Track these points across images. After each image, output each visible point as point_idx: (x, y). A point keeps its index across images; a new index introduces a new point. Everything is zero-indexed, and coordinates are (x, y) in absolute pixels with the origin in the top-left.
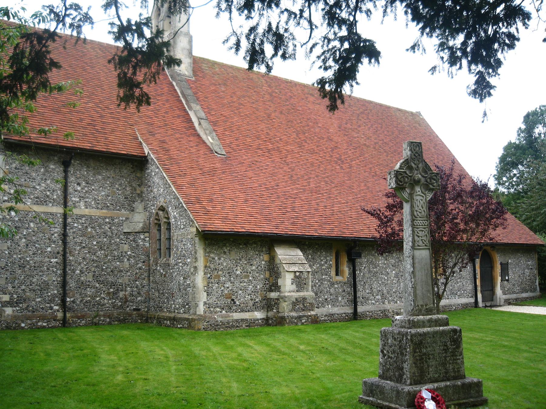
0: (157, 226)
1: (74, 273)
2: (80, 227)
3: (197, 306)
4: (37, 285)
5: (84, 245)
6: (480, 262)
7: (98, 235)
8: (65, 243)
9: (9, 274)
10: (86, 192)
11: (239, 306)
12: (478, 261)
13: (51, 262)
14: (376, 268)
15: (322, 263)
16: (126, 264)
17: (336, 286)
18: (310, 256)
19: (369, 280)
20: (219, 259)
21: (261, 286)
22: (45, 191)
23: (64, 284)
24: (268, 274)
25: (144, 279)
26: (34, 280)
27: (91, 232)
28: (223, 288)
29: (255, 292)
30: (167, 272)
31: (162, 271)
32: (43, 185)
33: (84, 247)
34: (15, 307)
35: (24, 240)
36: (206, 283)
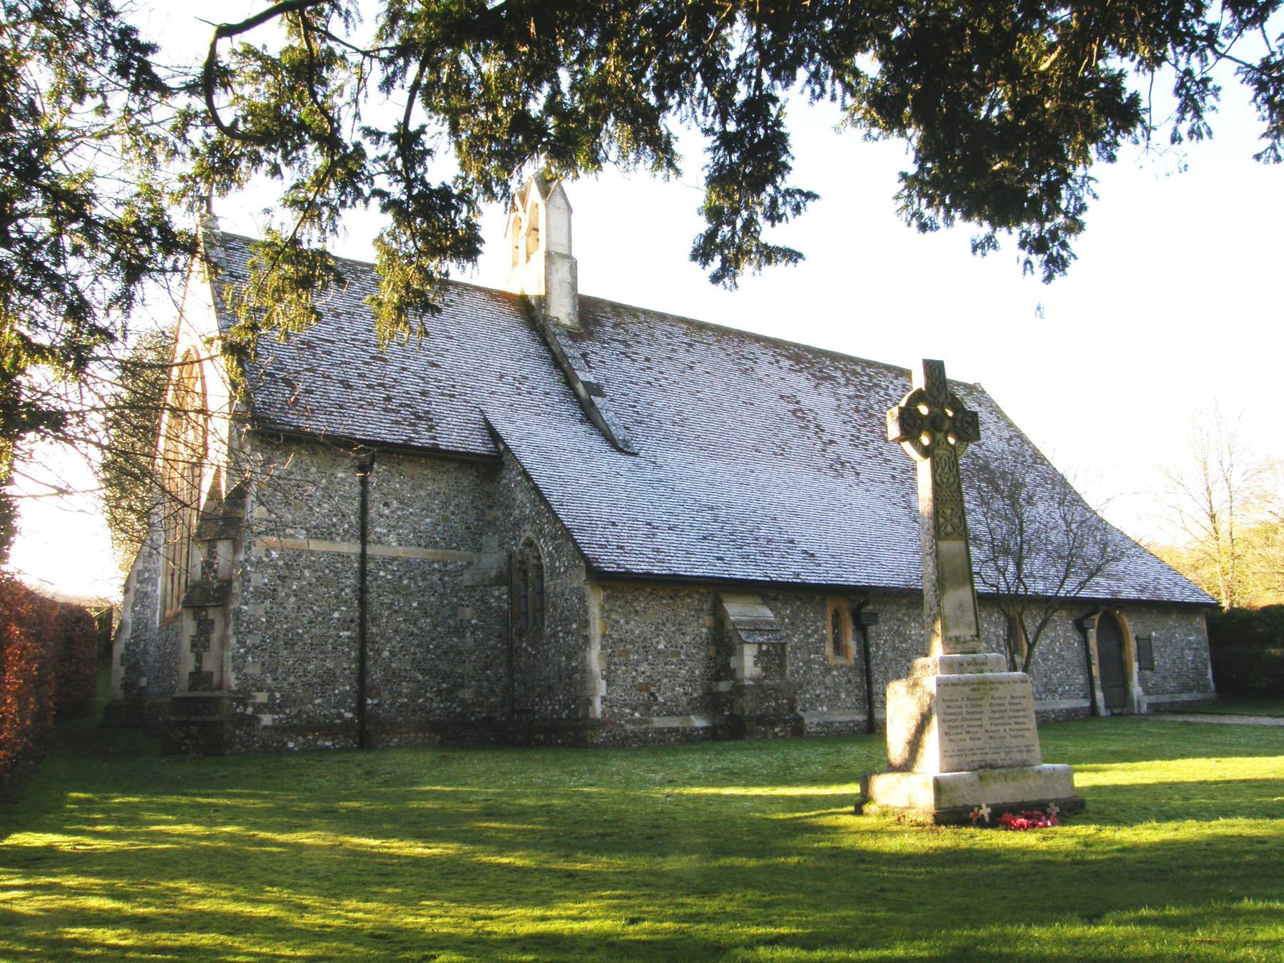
0: (521, 574)
1: (379, 655)
2: (389, 577)
3: (589, 702)
4: (315, 676)
5: (397, 608)
6: (1098, 635)
7: (419, 591)
8: (363, 603)
9: (266, 656)
10: (399, 517)
11: (664, 704)
12: (1092, 633)
13: (340, 637)
14: (906, 641)
15: (809, 632)
16: (469, 640)
17: (835, 673)
18: (787, 620)
19: (893, 663)
20: (627, 622)
21: (702, 671)
22: (329, 516)
23: (362, 674)
24: (712, 648)
25: (500, 665)
26: (311, 667)
27: (408, 586)
28: (634, 673)
29: (691, 681)
30: (538, 651)
31: (530, 649)
32: (326, 505)
33: (396, 612)
34: (277, 713)
35: (293, 599)
36: (604, 665)
